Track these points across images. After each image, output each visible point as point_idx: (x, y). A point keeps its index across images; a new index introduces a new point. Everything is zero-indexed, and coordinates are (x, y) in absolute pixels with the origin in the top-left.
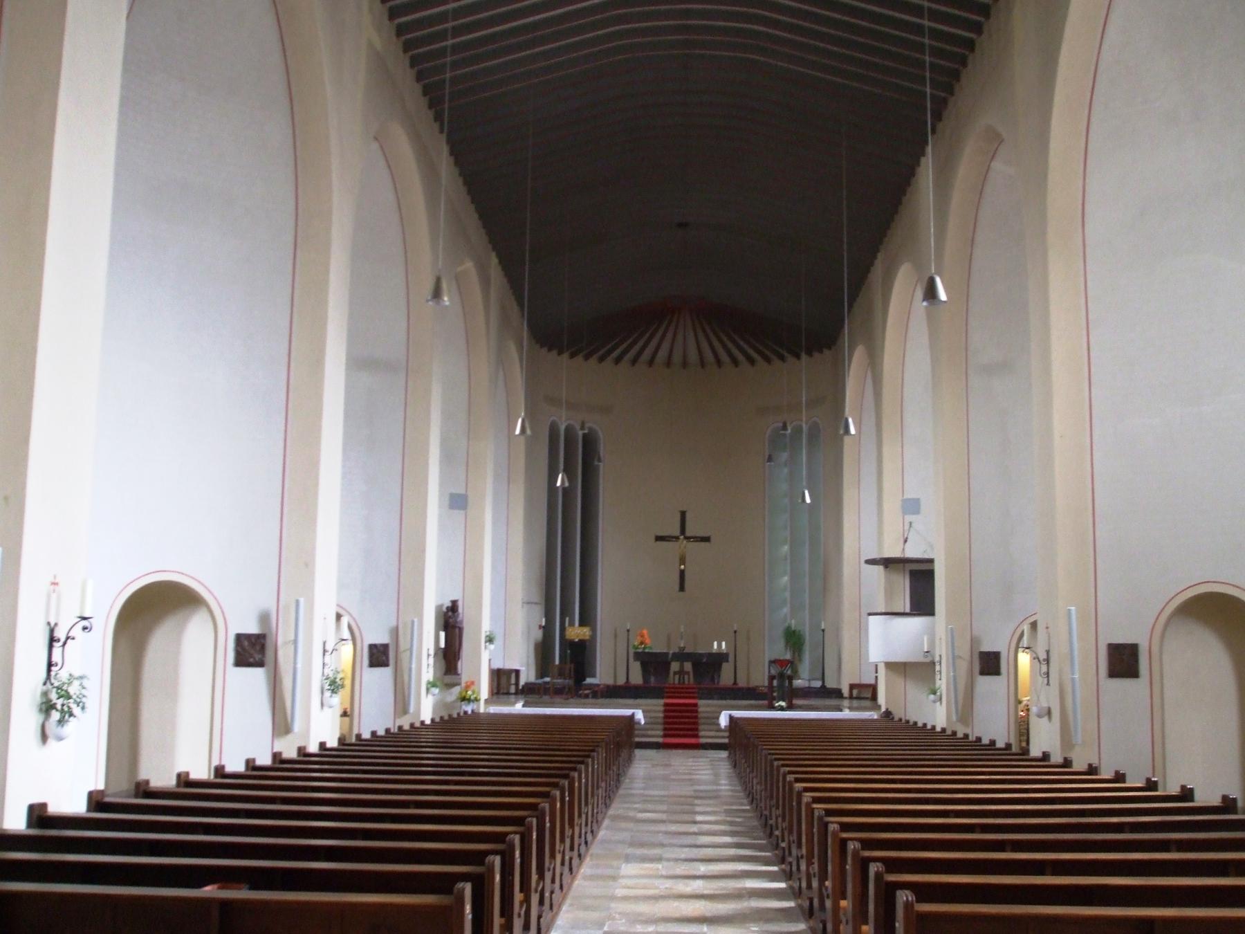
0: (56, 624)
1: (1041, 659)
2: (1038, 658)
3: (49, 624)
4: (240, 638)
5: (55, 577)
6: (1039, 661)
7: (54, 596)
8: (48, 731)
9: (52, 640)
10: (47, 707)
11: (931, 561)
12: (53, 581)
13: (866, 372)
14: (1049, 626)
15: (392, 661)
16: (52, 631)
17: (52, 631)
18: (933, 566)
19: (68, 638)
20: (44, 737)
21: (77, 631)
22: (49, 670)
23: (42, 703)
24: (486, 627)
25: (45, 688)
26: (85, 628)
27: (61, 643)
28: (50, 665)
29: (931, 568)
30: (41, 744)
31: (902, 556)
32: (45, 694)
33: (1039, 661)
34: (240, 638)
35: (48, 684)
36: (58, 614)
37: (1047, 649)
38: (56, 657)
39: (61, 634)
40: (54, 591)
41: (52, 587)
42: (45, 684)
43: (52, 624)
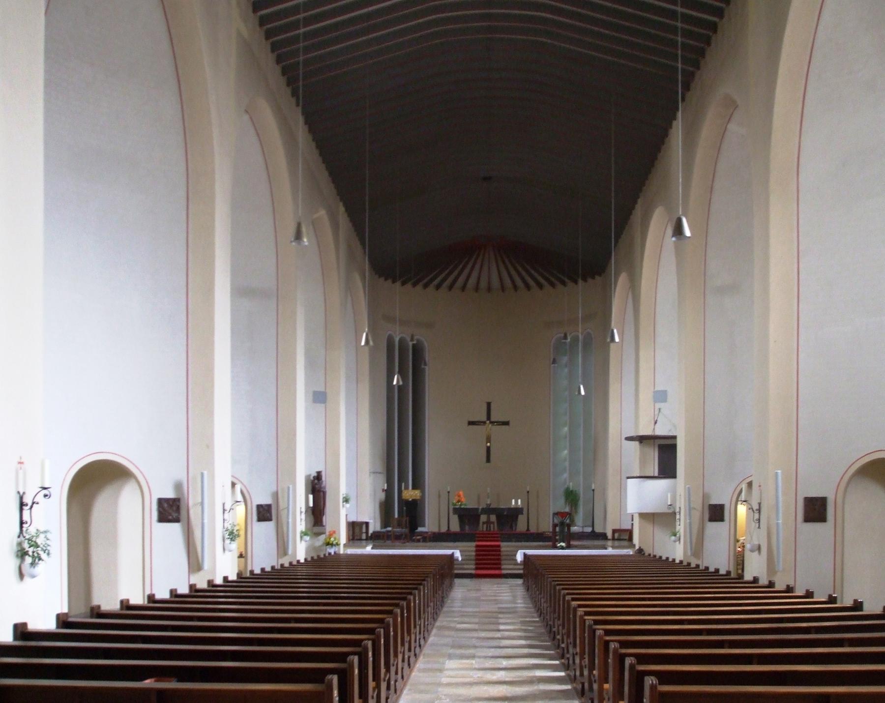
0: (24, 493)
1: (755, 509)
2: (752, 509)
3: (19, 492)
4: (161, 501)
5: (21, 458)
6: (753, 511)
7: (21, 472)
9: (22, 505)
12: (19, 461)
15: (274, 517)
16: (21, 498)
17: (21, 498)
19: (33, 503)
20: (21, 575)
21: (40, 498)
22: (21, 527)
23: (18, 551)
24: (343, 491)
25: (19, 540)
26: (45, 496)
27: (28, 507)
28: (22, 523)
32: (20, 544)
33: (753, 511)
34: (161, 501)
35: (21, 537)
38: (26, 517)
39: (28, 500)
40: (21, 468)
42: (19, 537)
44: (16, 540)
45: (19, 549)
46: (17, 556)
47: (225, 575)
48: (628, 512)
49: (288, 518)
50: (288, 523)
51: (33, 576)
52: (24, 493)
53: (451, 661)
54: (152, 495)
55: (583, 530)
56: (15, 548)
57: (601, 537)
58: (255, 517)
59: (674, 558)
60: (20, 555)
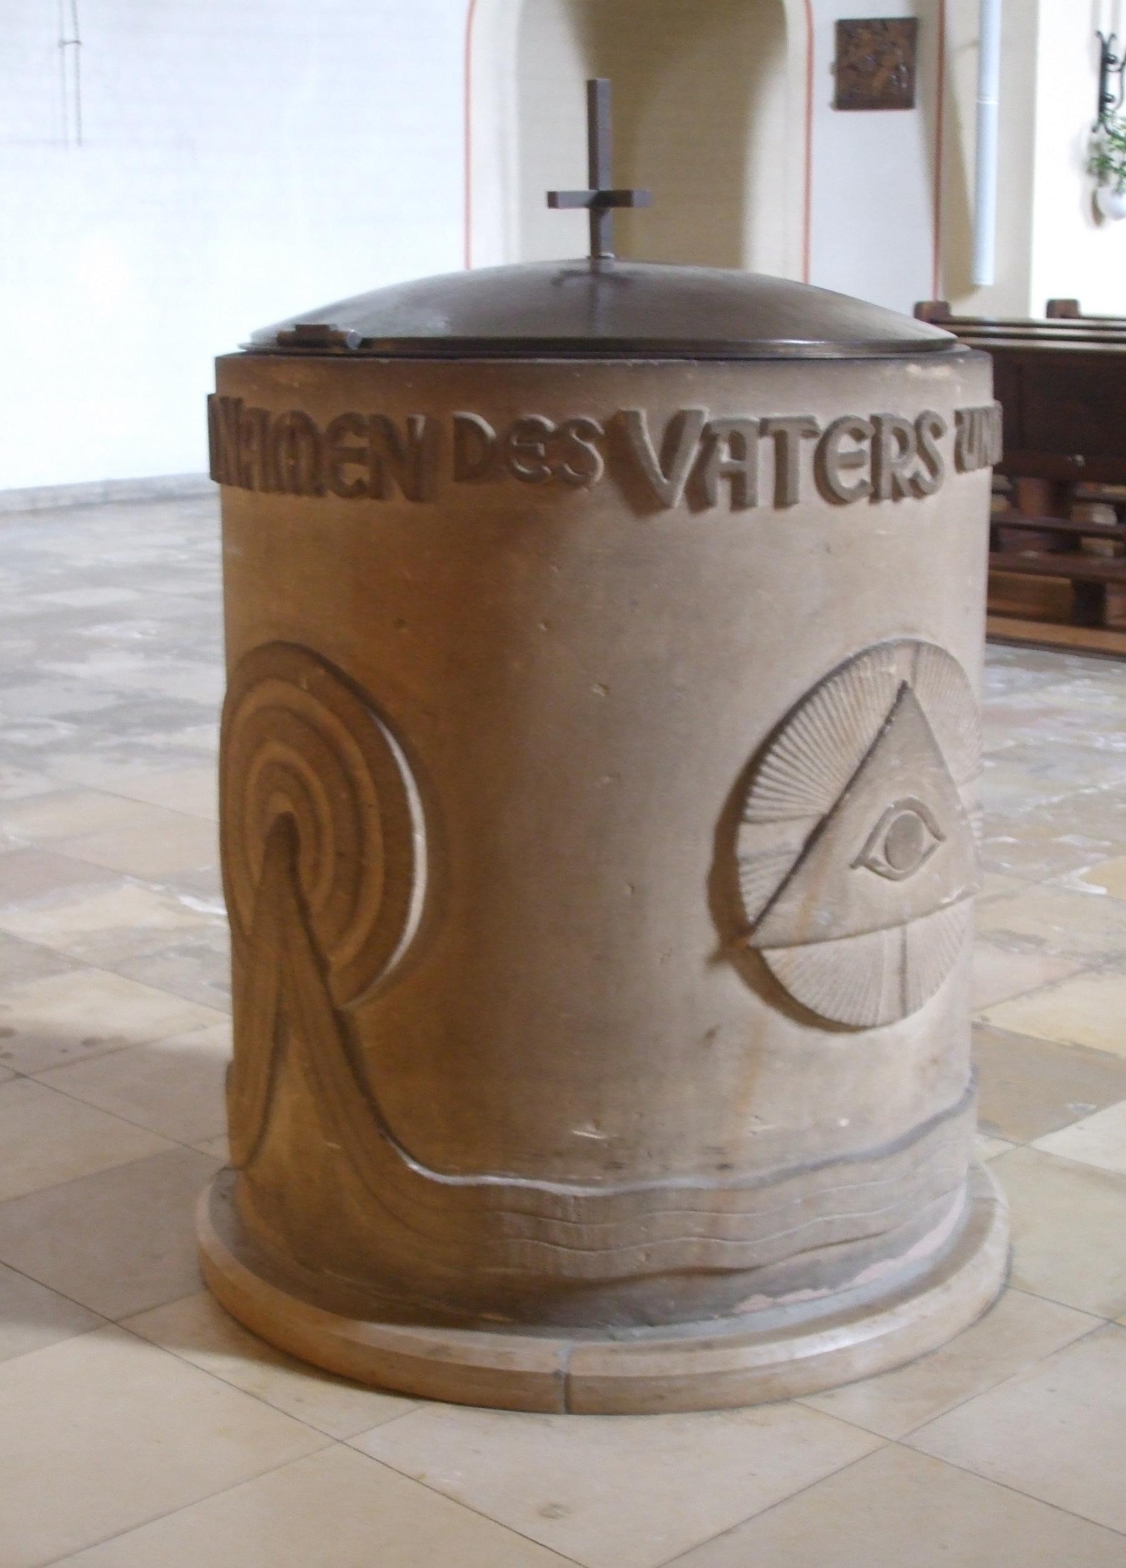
0: (1113, 36)
3: (1099, 34)
15: (923, 85)
16: (1105, 47)
20: (1098, 215)
22: (1102, 109)
25: (1096, 137)
28: (1104, 99)
32: (1096, 146)
35: (1102, 130)
42: (1094, 130)
44: (1086, 136)
45: (1096, 155)
46: (1090, 171)
48: (1115, 524)
49: (980, 93)
50: (980, 110)
51: (1119, 215)
52: (1113, 36)
56: (1084, 152)
57: (841, 1163)
58: (826, 86)
60: (1096, 170)
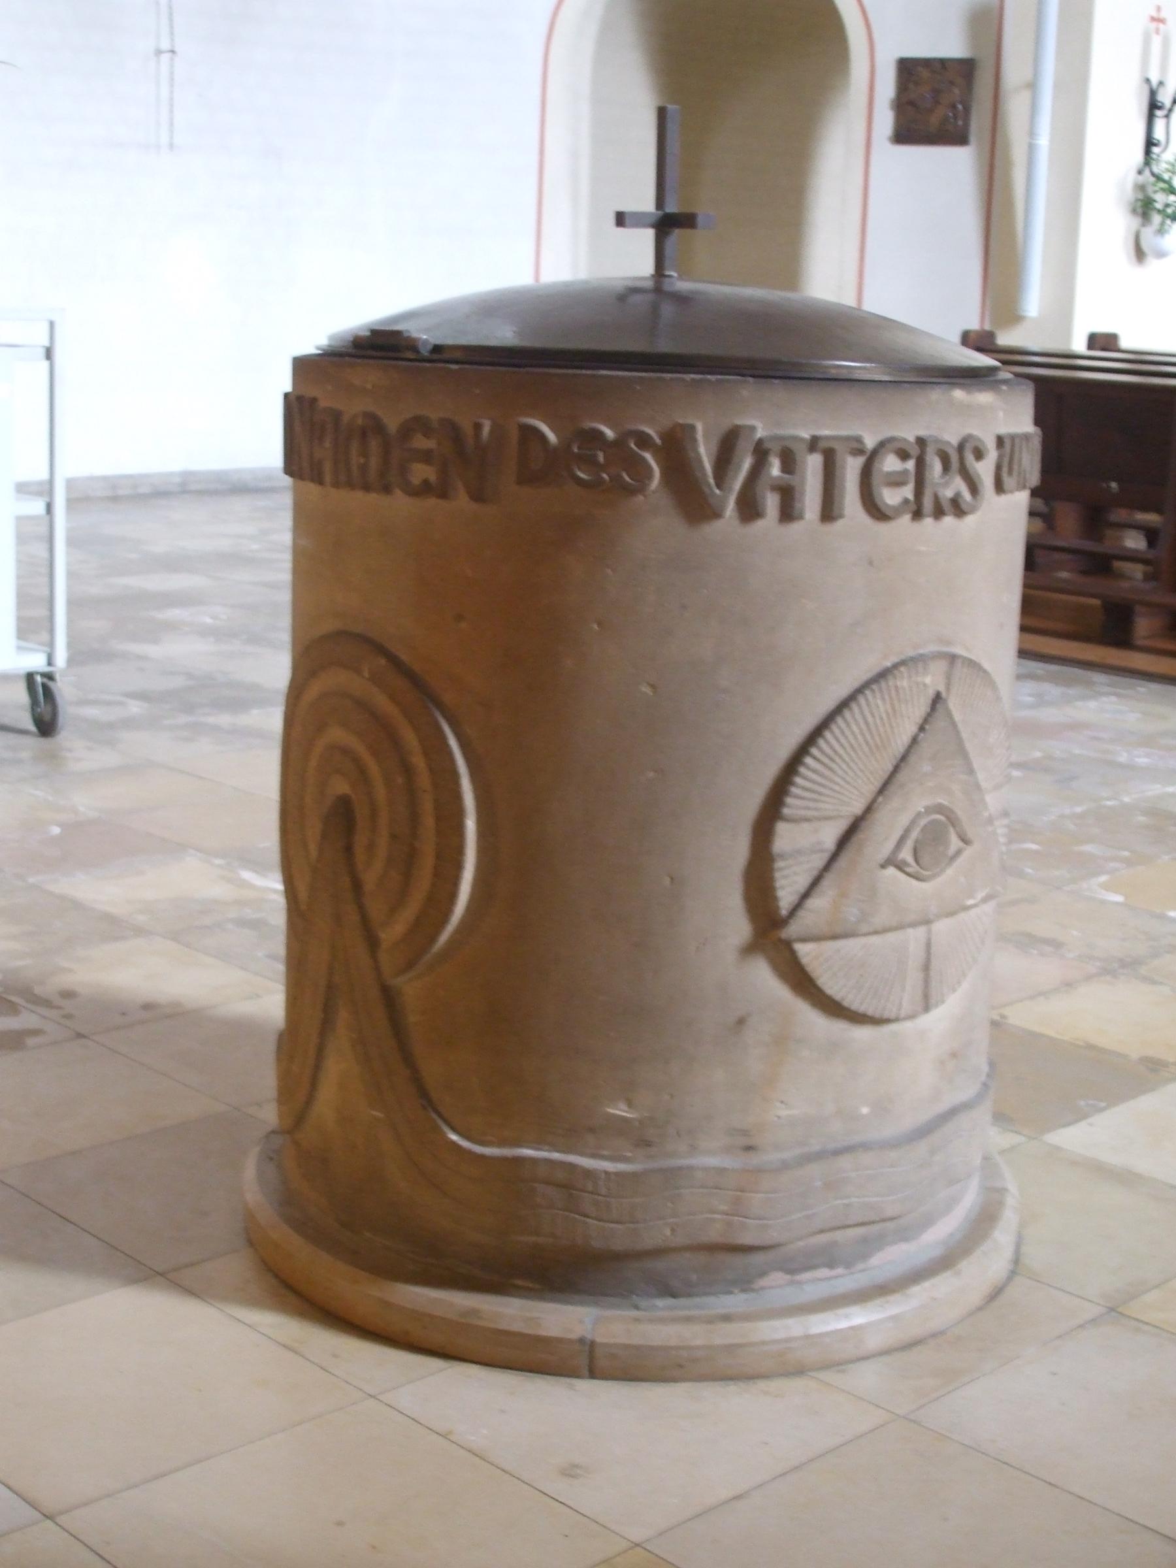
0: (1161, 83)
3: (1148, 81)
4: (908, 69)
5: (1159, 9)
7: (1156, 43)
8: (1145, 245)
9: (1154, 106)
10: (1144, 208)
11: (1019, 677)
12: (1154, 14)
13: (810, 1376)
14: (176, 49)
15: (978, 123)
16: (1153, 94)
18: (1021, 641)
20: (1140, 254)
22: (1148, 152)
23: (1137, 200)
25: (1141, 179)
27: (1164, 112)
28: (1150, 143)
29: (1026, 589)
30: (1134, 258)
31: (849, 300)
32: (1141, 188)
34: (908, 69)
35: (1147, 172)
36: (1164, 67)
37: (47, 344)
38: (1159, 133)
40: (1157, 32)
41: (1153, 25)
42: (1140, 172)
43: (1154, 82)
44: (1131, 178)
47: (622, 210)
49: (1032, 133)
50: (1031, 149)
53: (797, 459)
54: (878, 47)
55: (1167, 200)
56: (1129, 193)
59: (700, 220)
60: (1139, 210)
